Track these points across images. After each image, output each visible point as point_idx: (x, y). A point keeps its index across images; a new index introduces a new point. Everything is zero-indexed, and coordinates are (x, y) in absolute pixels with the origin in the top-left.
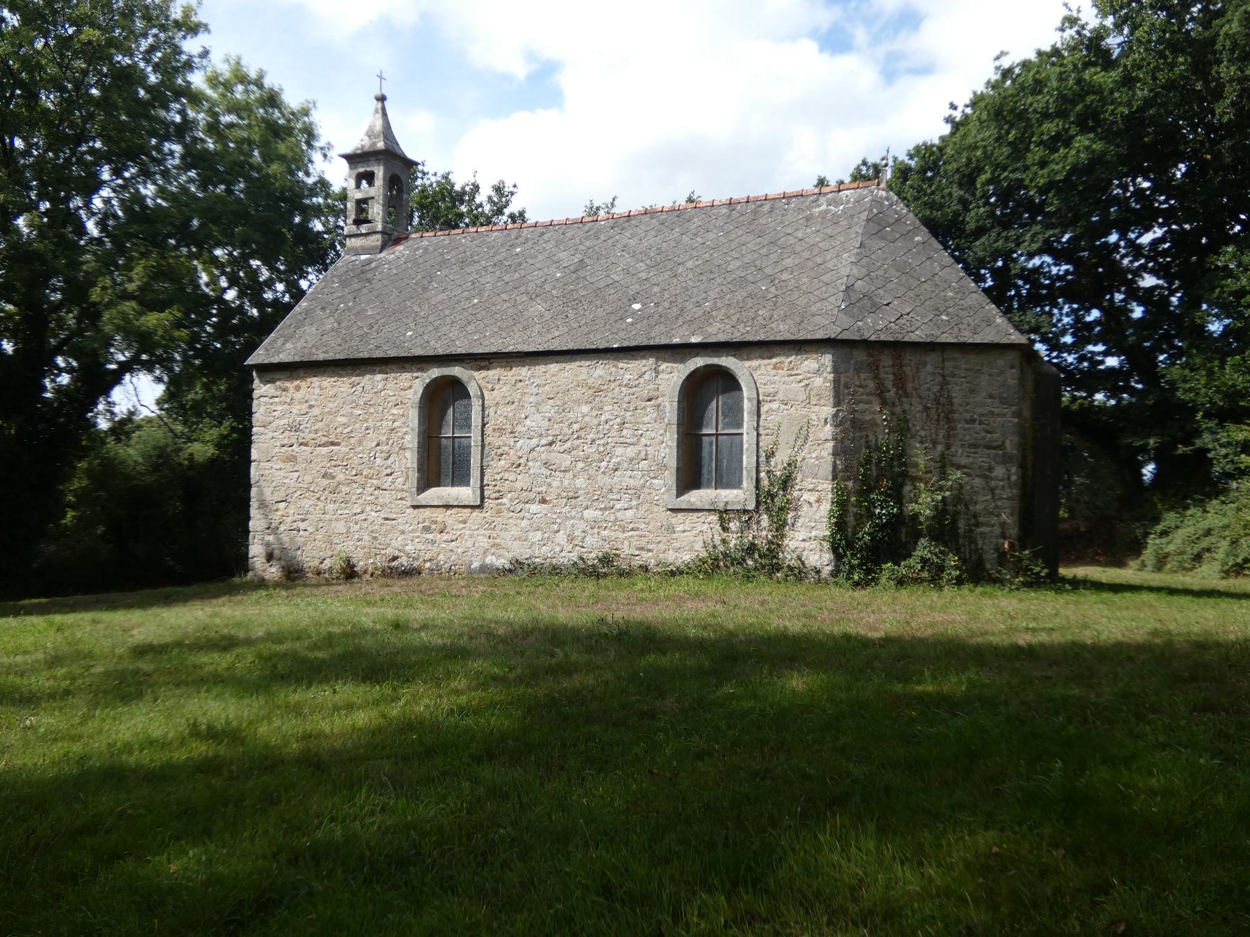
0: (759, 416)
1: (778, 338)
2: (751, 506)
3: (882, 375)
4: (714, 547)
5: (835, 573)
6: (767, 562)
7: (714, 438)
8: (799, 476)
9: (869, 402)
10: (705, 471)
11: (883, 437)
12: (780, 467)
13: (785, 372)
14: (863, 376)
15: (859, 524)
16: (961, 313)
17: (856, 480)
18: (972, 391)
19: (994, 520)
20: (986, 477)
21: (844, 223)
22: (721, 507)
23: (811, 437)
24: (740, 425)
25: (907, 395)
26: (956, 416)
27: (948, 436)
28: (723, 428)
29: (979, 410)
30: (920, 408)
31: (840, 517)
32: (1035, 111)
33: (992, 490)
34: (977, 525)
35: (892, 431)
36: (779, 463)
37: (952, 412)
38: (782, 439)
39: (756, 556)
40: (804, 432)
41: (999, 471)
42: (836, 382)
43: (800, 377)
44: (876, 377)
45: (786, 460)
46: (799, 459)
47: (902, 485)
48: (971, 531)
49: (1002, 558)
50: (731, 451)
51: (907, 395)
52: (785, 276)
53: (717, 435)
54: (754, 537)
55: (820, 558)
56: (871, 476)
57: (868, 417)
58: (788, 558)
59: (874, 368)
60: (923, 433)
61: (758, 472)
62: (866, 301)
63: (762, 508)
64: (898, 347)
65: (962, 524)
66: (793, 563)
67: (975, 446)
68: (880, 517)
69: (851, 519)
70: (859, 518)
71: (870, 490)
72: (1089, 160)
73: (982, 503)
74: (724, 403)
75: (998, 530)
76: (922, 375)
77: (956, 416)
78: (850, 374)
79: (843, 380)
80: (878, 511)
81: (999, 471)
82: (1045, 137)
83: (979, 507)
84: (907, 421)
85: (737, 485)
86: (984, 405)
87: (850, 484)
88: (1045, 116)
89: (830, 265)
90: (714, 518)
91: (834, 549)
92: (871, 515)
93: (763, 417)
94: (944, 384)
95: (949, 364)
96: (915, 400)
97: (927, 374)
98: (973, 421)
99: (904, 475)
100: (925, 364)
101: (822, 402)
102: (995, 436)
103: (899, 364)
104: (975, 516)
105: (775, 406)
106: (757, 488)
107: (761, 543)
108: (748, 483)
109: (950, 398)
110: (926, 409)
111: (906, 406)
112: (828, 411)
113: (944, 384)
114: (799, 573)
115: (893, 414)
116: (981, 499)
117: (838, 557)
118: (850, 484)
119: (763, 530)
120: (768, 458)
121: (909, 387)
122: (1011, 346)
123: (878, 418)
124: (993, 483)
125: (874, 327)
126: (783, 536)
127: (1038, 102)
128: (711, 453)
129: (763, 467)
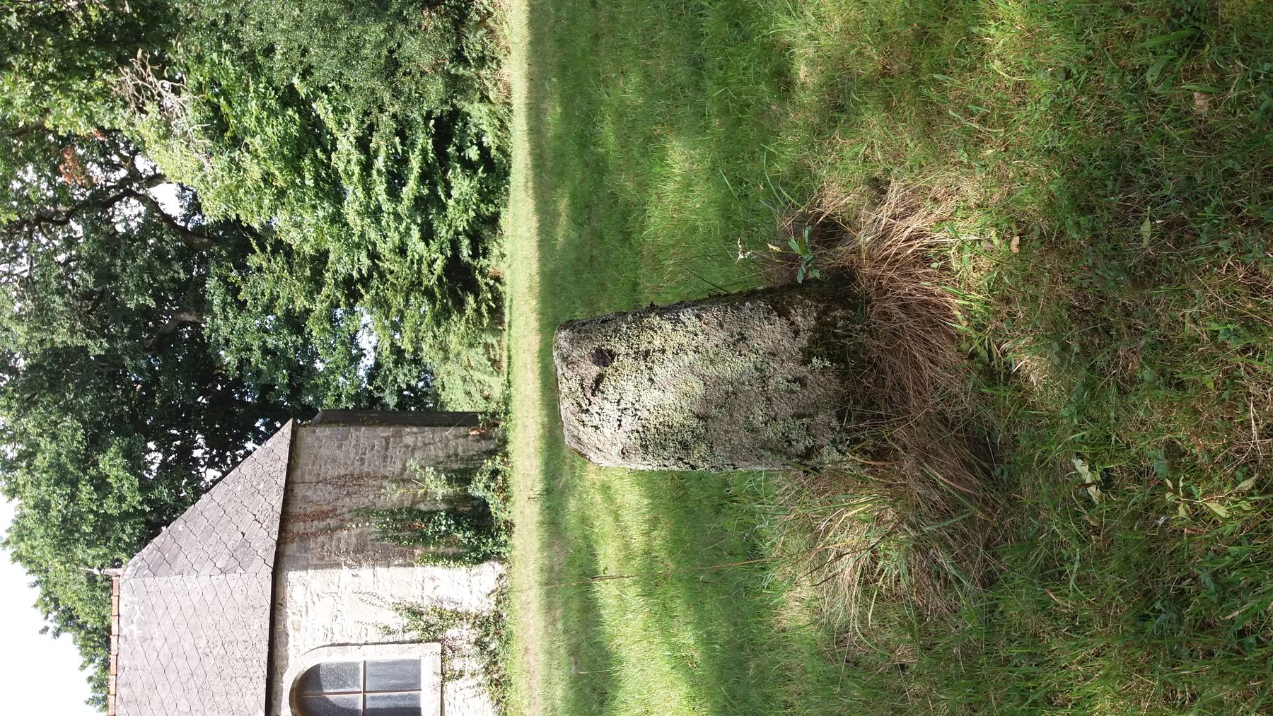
0: (347, 644)
1: (268, 626)
2: (437, 647)
3: (313, 530)
4: (479, 685)
5: (502, 560)
6: (492, 627)
7: (368, 695)
8: (410, 599)
9: (339, 540)
10: (401, 704)
11: (373, 527)
12: (399, 619)
13: (304, 619)
14: (312, 545)
15: (457, 543)
16: (259, 474)
17: (413, 547)
18: (334, 461)
19: (452, 443)
20: (414, 449)
21: (154, 599)
22: (439, 679)
23: (370, 589)
24: (354, 667)
25: (335, 510)
26: (356, 472)
27: (376, 478)
28: (358, 686)
29: (352, 456)
30: (347, 499)
31: (449, 558)
32: (66, 507)
33: (425, 445)
34: (456, 455)
35: (369, 520)
36: (397, 621)
37: (352, 475)
38: (372, 619)
39: (487, 639)
40: (365, 597)
41: (409, 440)
42: (316, 567)
43: (310, 604)
44: (315, 535)
45: (393, 613)
46: (391, 600)
47: (420, 511)
48: (462, 459)
49: (482, 437)
50: (383, 676)
51: (335, 510)
52: (203, 643)
53: (364, 691)
54: (469, 642)
55: (488, 573)
56: (409, 533)
57: (354, 540)
58: (487, 607)
59: (304, 537)
60: (371, 497)
61: (404, 642)
62: (238, 554)
63: (440, 637)
64: (286, 517)
65: (455, 466)
66: (493, 598)
67: (385, 457)
68: (449, 526)
69: (450, 551)
70: (448, 545)
71: (424, 536)
72: (124, 457)
73: (437, 452)
74: (332, 686)
75: (462, 440)
76: (315, 498)
77: (356, 472)
78: (310, 556)
79: (315, 562)
80: (443, 528)
81: (409, 440)
82: (95, 496)
83: (441, 453)
84: (359, 509)
85: (416, 663)
86: (348, 452)
87: (417, 552)
88: (72, 497)
89: (196, 598)
90: (450, 686)
91: (479, 561)
92: (447, 534)
93: (348, 641)
94: (326, 482)
95: (307, 478)
96: (340, 503)
97: (312, 496)
98: (362, 460)
99: (410, 510)
100: (305, 497)
101: (336, 580)
102: (376, 443)
103: (305, 517)
104: (449, 457)
105: (337, 629)
106: (420, 642)
107: (474, 634)
108: (414, 652)
109: (339, 477)
110: (348, 494)
111: (345, 510)
112: (345, 573)
113: (326, 482)
114: (502, 596)
115: (351, 520)
116: (433, 452)
117: (487, 557)
118: (417, 552)
119: (463, 634)
120: (390, 633)
121: (325, 508)
122: (294, 433)
123: (355, 531)
124: (420, 444)
125: (265, 540)
126: (467, 613)
127: (58, 504)
128: (383, 698)
129: (399, 637)
